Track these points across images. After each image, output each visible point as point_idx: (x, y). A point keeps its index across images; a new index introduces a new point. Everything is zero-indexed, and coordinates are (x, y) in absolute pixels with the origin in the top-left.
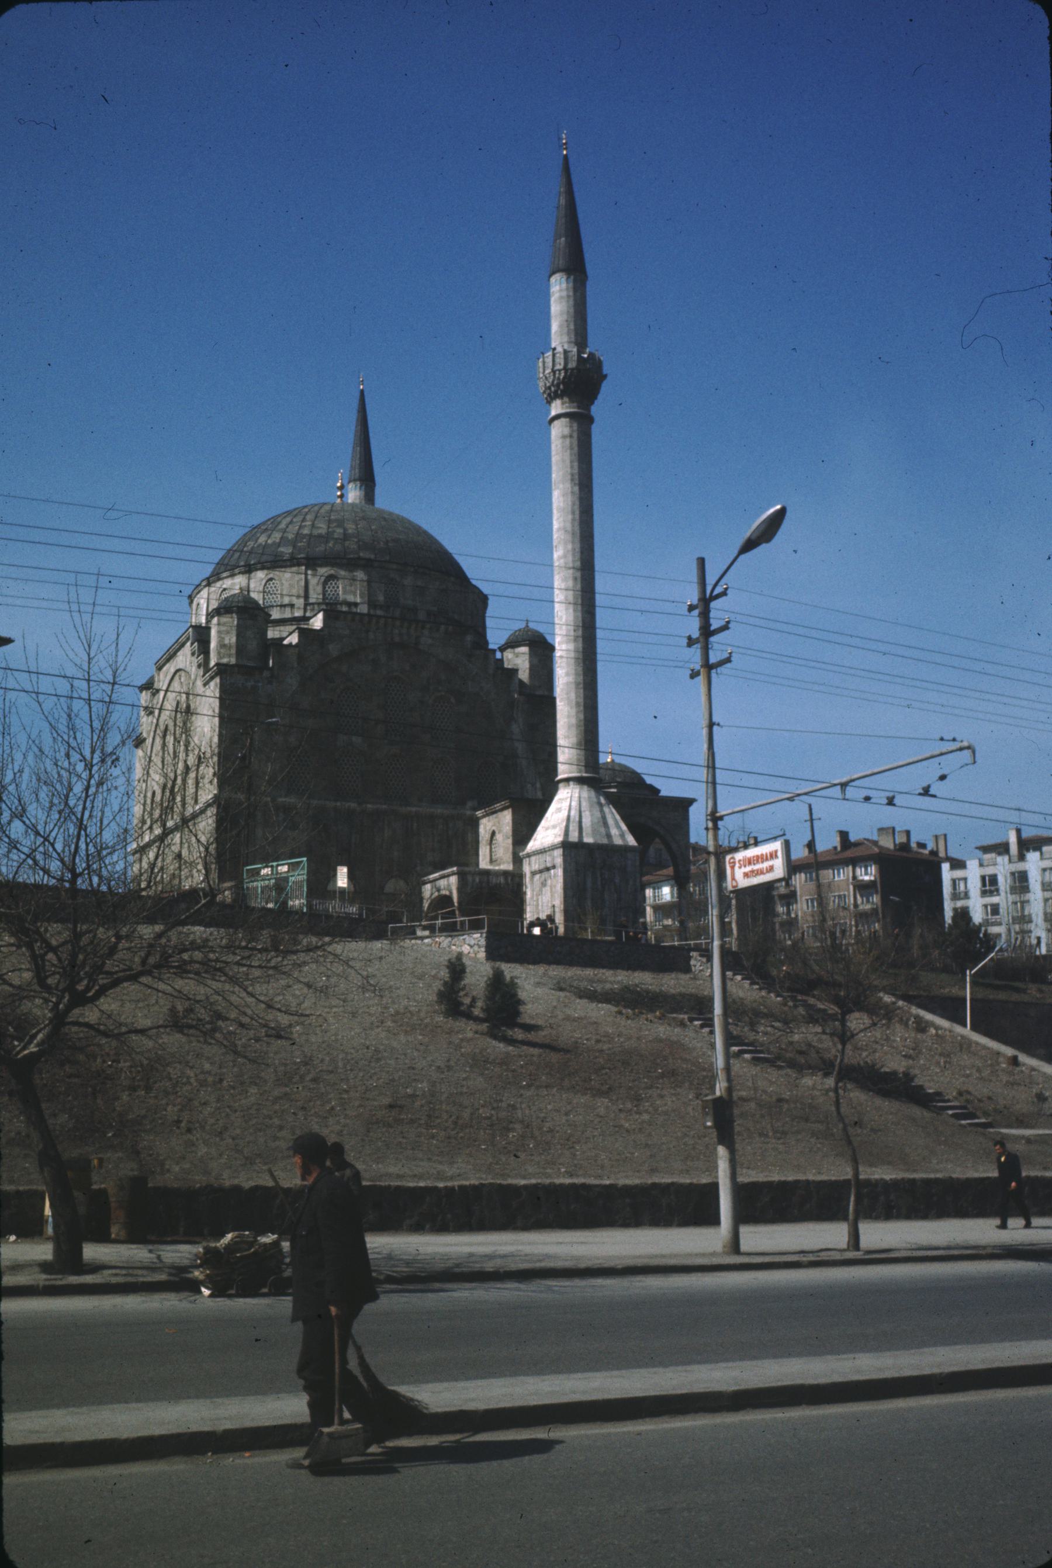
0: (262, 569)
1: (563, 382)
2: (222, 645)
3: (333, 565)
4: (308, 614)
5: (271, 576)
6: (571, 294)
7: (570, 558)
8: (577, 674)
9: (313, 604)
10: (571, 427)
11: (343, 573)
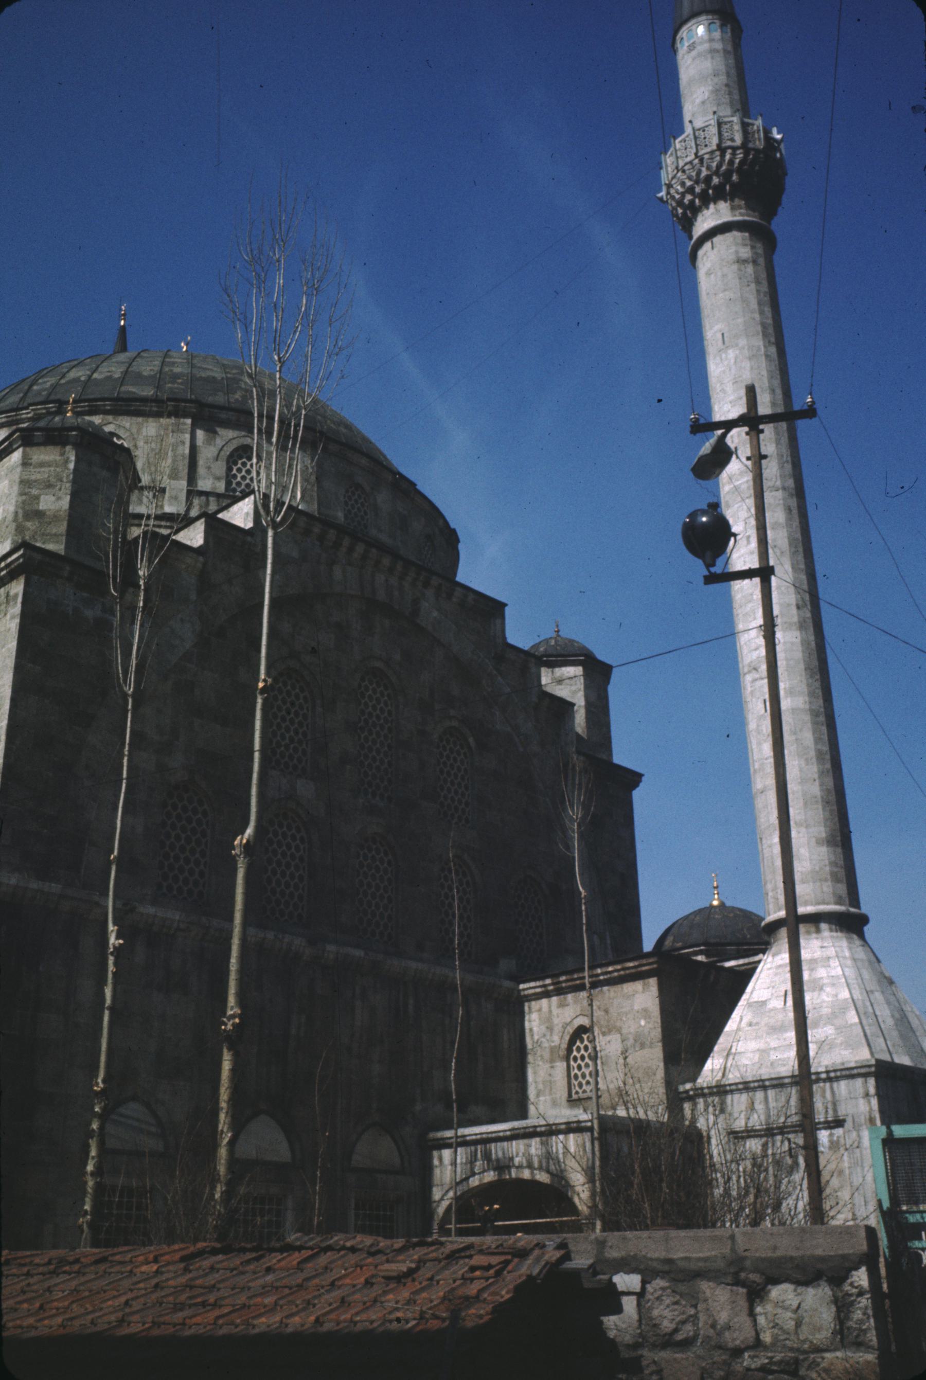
1: (739, 170)
6: (730, 48)
8: (811, 694)
9: (207, 494)
10: (753, 247)
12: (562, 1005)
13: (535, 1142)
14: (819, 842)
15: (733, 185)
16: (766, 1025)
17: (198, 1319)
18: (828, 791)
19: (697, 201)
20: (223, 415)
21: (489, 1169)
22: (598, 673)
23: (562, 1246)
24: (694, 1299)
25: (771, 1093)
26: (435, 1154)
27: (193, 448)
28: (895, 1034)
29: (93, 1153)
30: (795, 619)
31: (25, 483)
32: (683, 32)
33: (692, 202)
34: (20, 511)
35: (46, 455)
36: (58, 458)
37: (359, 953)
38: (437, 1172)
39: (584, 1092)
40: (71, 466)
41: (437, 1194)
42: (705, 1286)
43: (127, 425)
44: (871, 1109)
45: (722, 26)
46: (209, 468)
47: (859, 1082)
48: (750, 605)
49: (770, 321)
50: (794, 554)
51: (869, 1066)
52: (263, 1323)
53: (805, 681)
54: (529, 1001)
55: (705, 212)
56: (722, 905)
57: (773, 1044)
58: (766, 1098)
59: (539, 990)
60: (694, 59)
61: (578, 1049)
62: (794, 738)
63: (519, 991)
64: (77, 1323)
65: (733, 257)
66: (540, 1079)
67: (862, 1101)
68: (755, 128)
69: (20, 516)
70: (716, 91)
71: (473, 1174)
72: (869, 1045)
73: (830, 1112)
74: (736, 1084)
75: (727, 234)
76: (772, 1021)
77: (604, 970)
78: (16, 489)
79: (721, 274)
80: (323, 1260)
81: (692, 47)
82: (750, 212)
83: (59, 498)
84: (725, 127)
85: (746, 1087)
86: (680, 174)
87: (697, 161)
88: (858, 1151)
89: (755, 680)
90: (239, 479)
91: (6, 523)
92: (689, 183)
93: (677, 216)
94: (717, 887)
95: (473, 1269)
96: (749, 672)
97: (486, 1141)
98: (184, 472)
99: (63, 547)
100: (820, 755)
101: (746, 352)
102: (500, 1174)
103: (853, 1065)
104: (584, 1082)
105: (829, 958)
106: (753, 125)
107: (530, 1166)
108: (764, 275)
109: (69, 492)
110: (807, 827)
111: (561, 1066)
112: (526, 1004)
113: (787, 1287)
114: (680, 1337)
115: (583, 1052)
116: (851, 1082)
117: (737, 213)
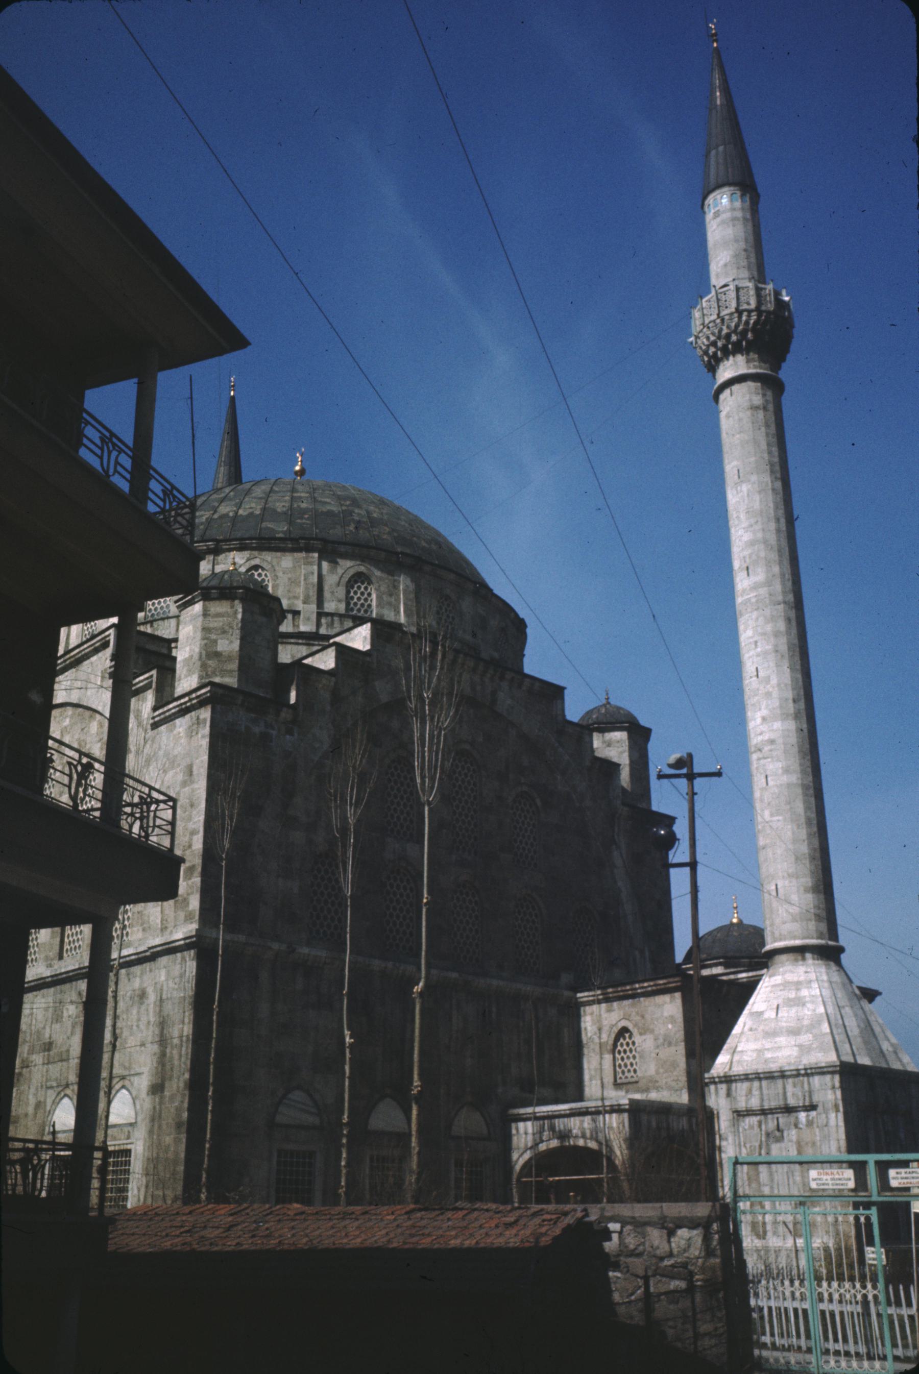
0: (241, 549)
1: (754, 330)
2: (210, 654)
3: (363, 559)
4: (323, 631)
5: (256, 562)
6: (748, 216)
7: (778, 587)
8: (803, 772)
10: (764, 395)
11: (378, 573)
12: (609, 1011)
13: (587, 1119)
14: (806, 891)
15: (748, 342)
16: (763, 1030)
17: (424, 1241)
18: (815, 850)
19: (719, 353)
20: (342, 549)
21: (554, 1138)
22: (640, 736)
23: (585, 1210)
24: (644, 1235)
25: (764, 1083)
26: (513, 1125)
27: (320, 576)
28: (859, 1040)
29: (344, 1155)
30: (792, 711)
31: (206, 630)
32: (710, 200)
33: (715, 354)
34: (204, 653)
35: (219, 607)
36: (229, 610)
37: (454, 975)
38: (515, 1139)
39: (626, 1077)
40: (240, 616)
41: (515, 1156)
42: (649, 1229)
43: (269, 559)
44: (836, 1099)
45: (742, 196)
46: (332, 593)
47: (828, 1077)
48: (756, 698)
49: (776, 460)
50: (791, 657)
51: (835, 1066)
52: (454, 1243)
53: (798, 761)
54: (585, 1006)
55: (726, 362)
56: (740, 922)
57: (768, 1046)
58: (761, 1087)
59: (591, 998)
60: (718, 226)
61: (622, 1045)
62: (788, 807)
63: (577, 999)
64: (369, 1241)
65: (746, 404)
66: (592, 1067)
67: (830, 1092)
68: (767, 292)
69: (204, 656)
70: (736, 256)
71: (542, 1141)
72: (837, 1050)
73: (807, 1099)
74: (739, 1075)
75: (743, 384)
76: (767, 1028)
77: (642, 985)
78: (199, 635)
79: (738, 415)
80: (476, 1214)
81: (717, 215)
82: (763, 364)
83: (231, 642)
84: (741, 293)
85: (746, 1078)
86: (705, 330)
87: (718, 321)
88: (826, 1129)
89: (759, 759)
90: (355, 600)
91: (193, 660)
92: (712, 338)
93: (703, 361)
94: (736, 908)
95: (544, 1221)
96: (755, 752)
97: (551, 1117)
98: (314, 598)
99: (236, 680)
100: (808, 822)
101: (756, 486)
102: (561, 1142)
103: (823, 1065)
104: (626, 1070)
105: (810, 981)
106: (765, 289)
107: (584, 1136)
108: (772, 418)
109: (239, 637)
110: (797, 878)
111: (608, 1058)
112: (582, 1009)
113: (685, 1230)
114: (637, 1252)
115: (625, 1047)
116: (822, 1077)
117: (751, 365)
